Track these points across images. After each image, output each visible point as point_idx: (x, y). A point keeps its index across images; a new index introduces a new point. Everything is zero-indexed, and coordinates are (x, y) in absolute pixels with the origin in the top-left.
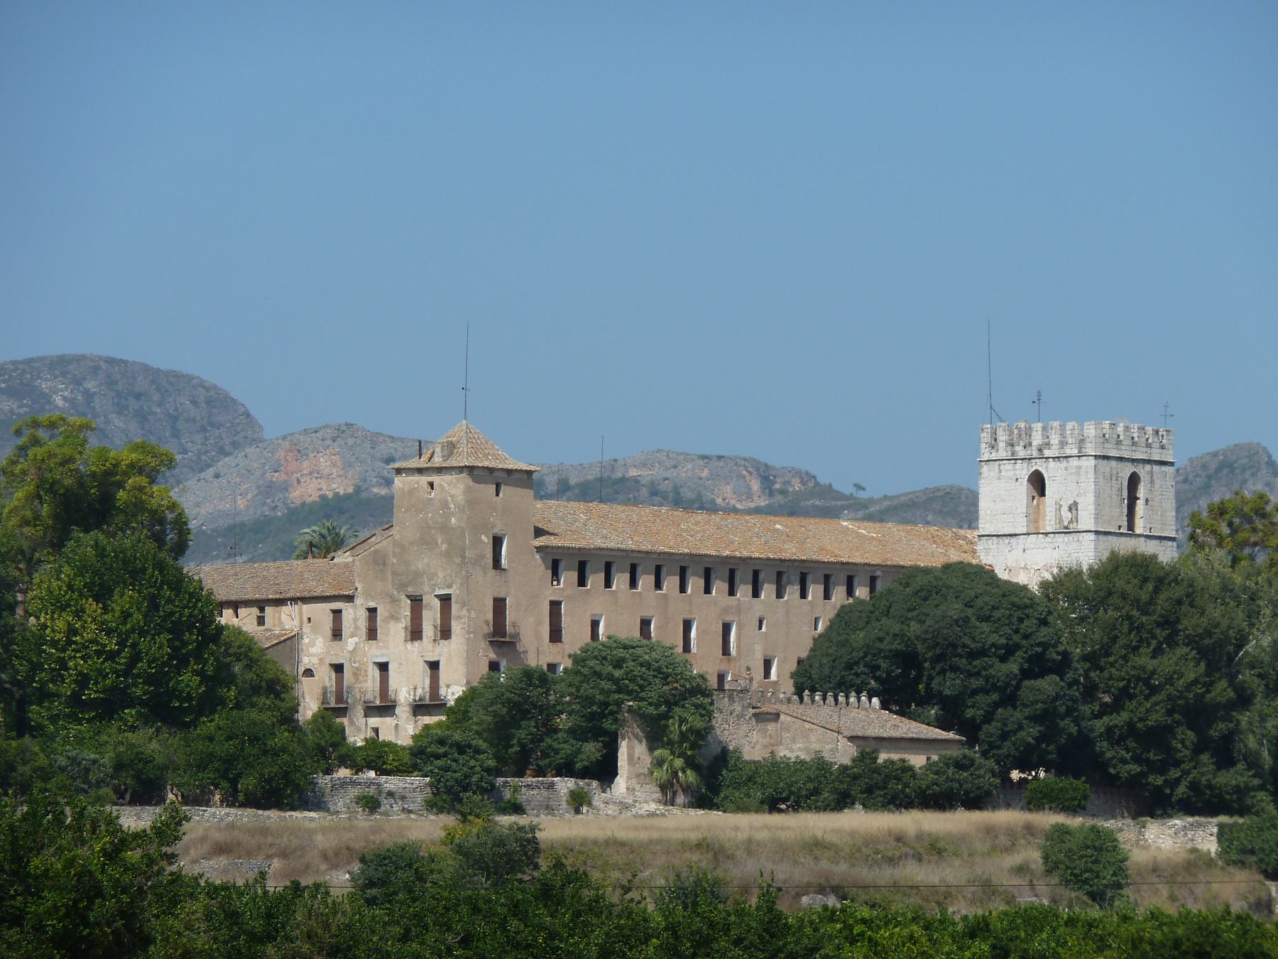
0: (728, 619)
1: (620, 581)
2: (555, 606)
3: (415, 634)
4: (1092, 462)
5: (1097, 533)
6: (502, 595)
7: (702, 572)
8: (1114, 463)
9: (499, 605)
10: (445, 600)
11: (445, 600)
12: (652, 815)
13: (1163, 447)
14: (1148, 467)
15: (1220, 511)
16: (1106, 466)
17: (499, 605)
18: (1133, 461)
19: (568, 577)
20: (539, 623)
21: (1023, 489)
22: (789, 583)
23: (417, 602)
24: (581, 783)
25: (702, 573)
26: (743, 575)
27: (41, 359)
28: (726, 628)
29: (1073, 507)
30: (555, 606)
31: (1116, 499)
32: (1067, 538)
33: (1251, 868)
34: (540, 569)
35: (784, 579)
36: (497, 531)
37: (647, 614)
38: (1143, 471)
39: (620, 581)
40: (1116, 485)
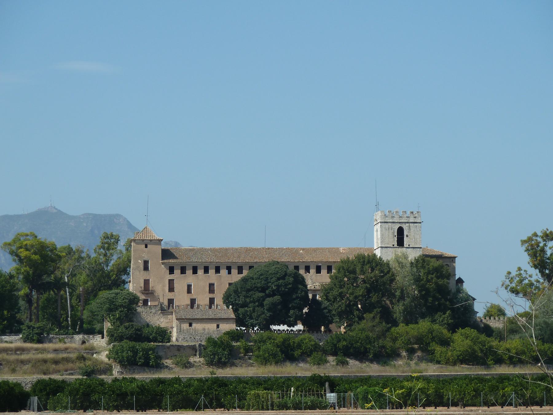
4: (380, 224)
5: (381, 247)
6: (148, 278)
8: (390, 224)
9: (147, 282)
12: (17, 349)
13: (415, 217)
14: (407, 225)
16: (387, 225)
18: (400, 223)
19: (177, 272)
20: (164, 286)
24: (86, 336)
27: (311, 249)
31: (391, 235)
33: (506, 363)
34: (164, 270)
36: (146, 258)
37: (212, 282)
38: (405, 227)
40: (391, 231)
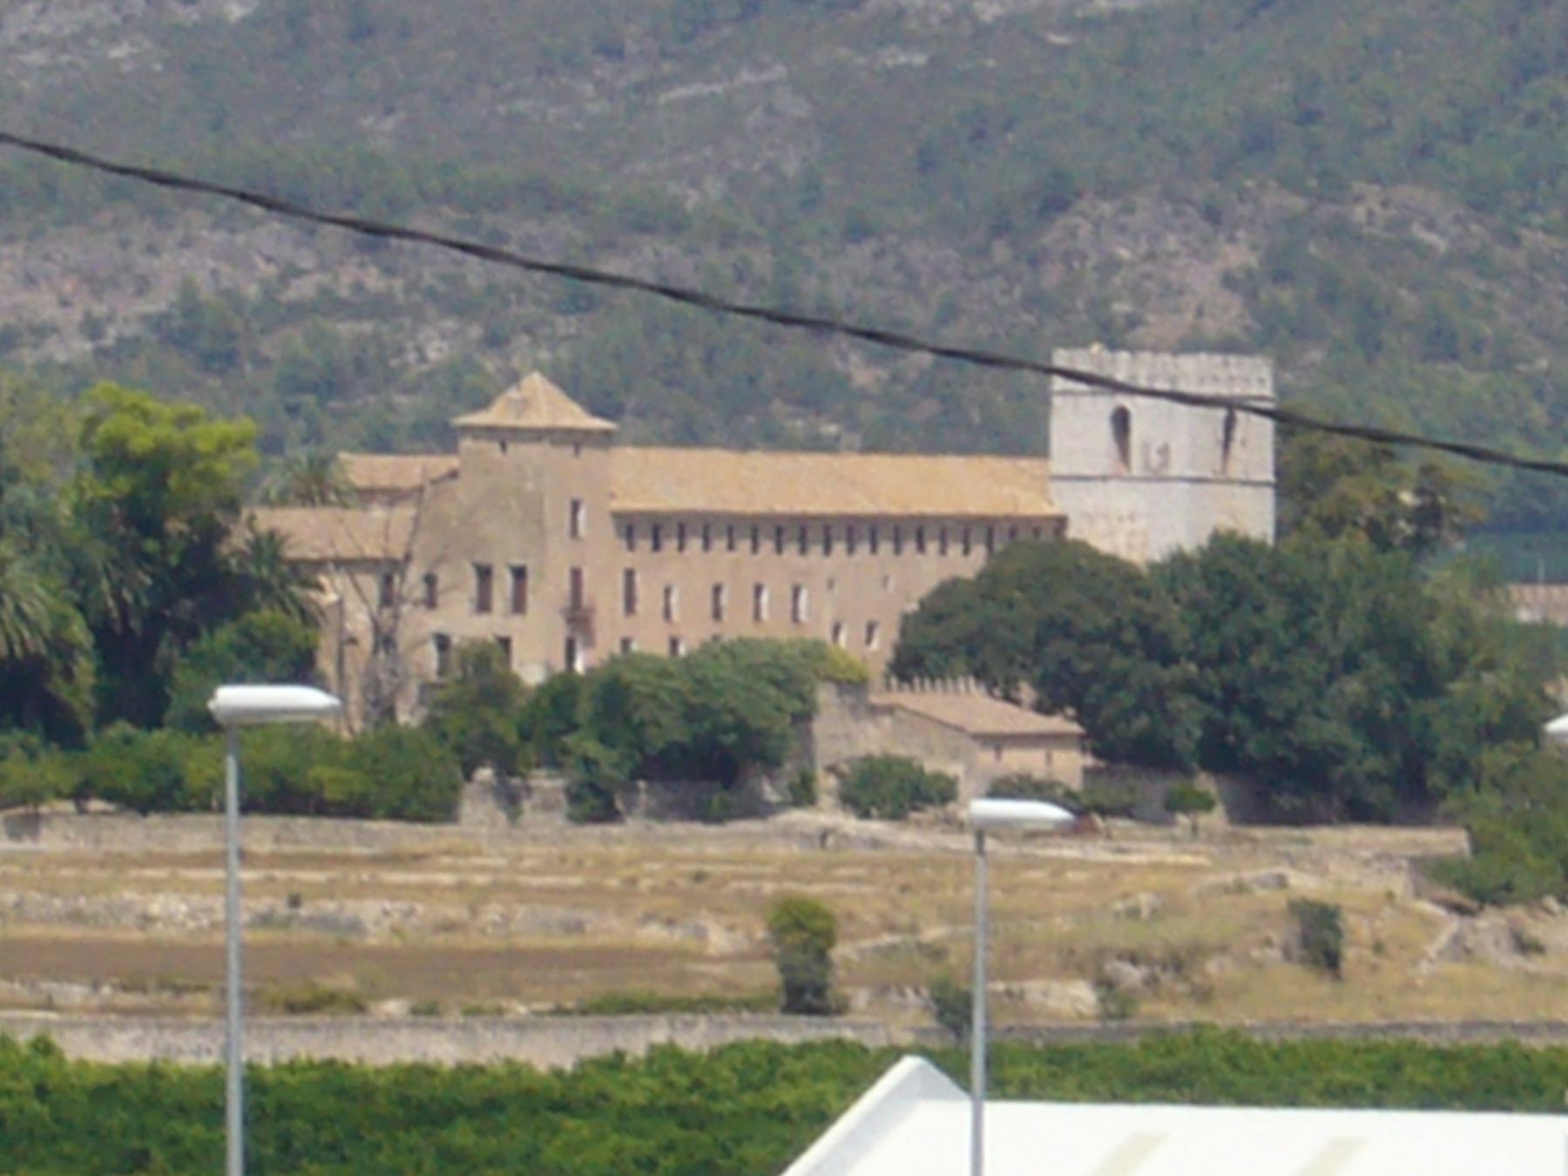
0: (800, 580)
1: (695, 544)
2: (630, 574)
3: (484, 605)
7: (773, 532)
9: (576, 574)
10: (520, 574)
11: (520, 574)
15: (1223, 573)
17: (576, 574)
21: (1105, 430)
22: (668, 536)
23: (485, 573)
25: (650, 533)
26: (815, 534)
28: (796, 592)
29: (1164, 451)
30: (630, 574)
32: (1157, 486)
35: (661, 534)
36: (576, 495)
37: (718, 579)
39: (695, 544)
